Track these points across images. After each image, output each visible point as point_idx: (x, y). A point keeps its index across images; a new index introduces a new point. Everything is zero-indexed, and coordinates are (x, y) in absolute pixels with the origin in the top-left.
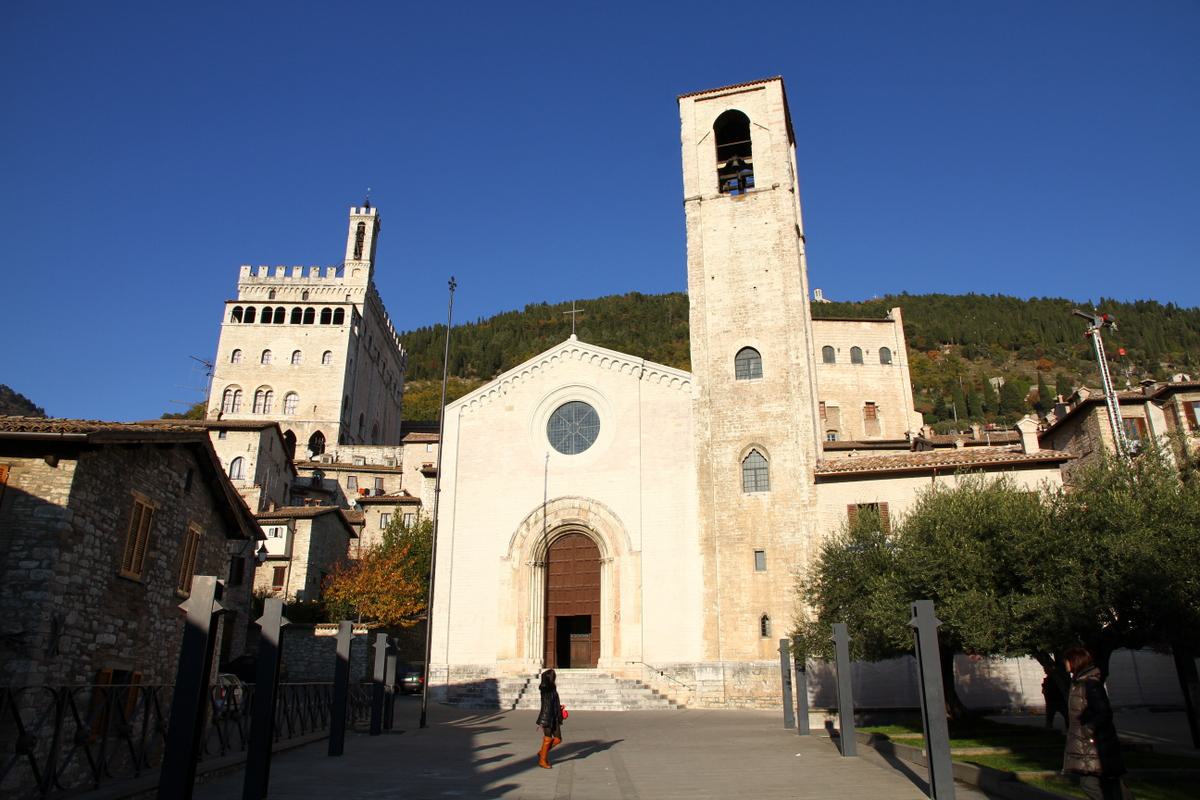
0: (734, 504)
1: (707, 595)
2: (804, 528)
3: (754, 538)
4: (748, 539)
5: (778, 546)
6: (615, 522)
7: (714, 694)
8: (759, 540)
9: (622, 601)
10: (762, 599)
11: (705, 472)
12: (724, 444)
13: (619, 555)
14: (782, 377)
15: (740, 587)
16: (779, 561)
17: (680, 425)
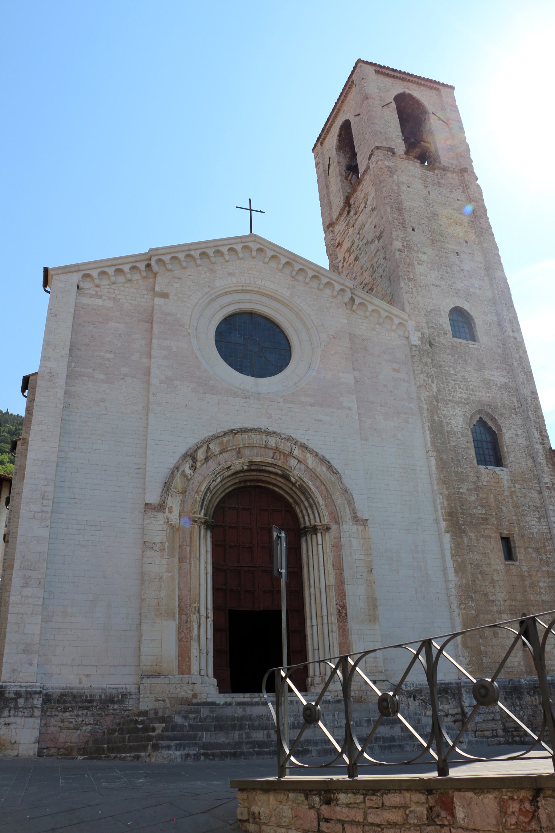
1: (460, 586)
3: (499, 519)
4: (493, 520)
5: (525, 532)
6: (329, 475)
7: (491, 725)
8: (505, 524)
9: (349, 590)
10: (519, 597)
12: (452, 404)
13: (337, 523)
14: (499, 347)
15: (493, 579)
16: (530, 550)
17: (397, 371)
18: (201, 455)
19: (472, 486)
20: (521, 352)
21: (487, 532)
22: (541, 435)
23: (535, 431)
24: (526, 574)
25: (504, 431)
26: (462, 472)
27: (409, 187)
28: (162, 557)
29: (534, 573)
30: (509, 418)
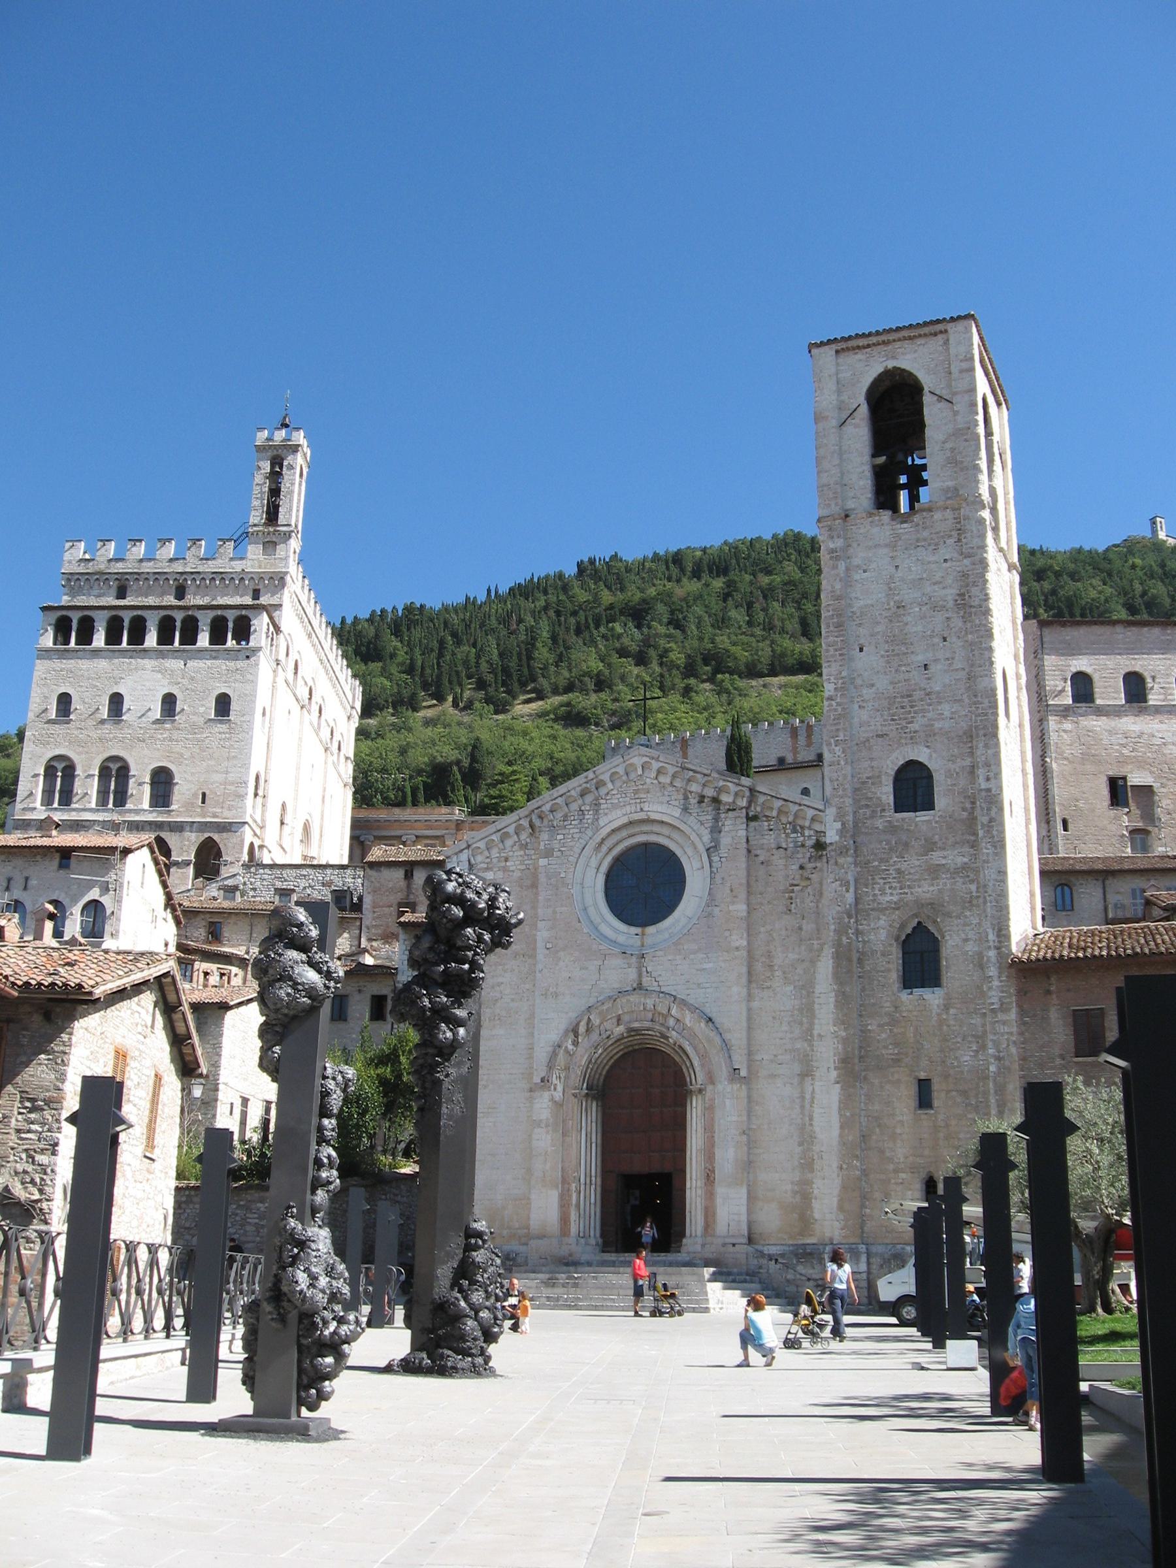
0: (887, 1006)
2: (990, 1045)
5: (952, 1072)
11: (851, 962)
14: (964, 809)
18: (582, 1029)
19: (886, 1020)
20: (994, 810)
21: (896, 1076)
22: (998, 936)
23: (990, 931)
24: (942, 1124)
25: (947, 938)
26: (874, 1004)
27: (865, 571)
28: (547, 1132)
29: (953, 1122)
30: (958, 917)
